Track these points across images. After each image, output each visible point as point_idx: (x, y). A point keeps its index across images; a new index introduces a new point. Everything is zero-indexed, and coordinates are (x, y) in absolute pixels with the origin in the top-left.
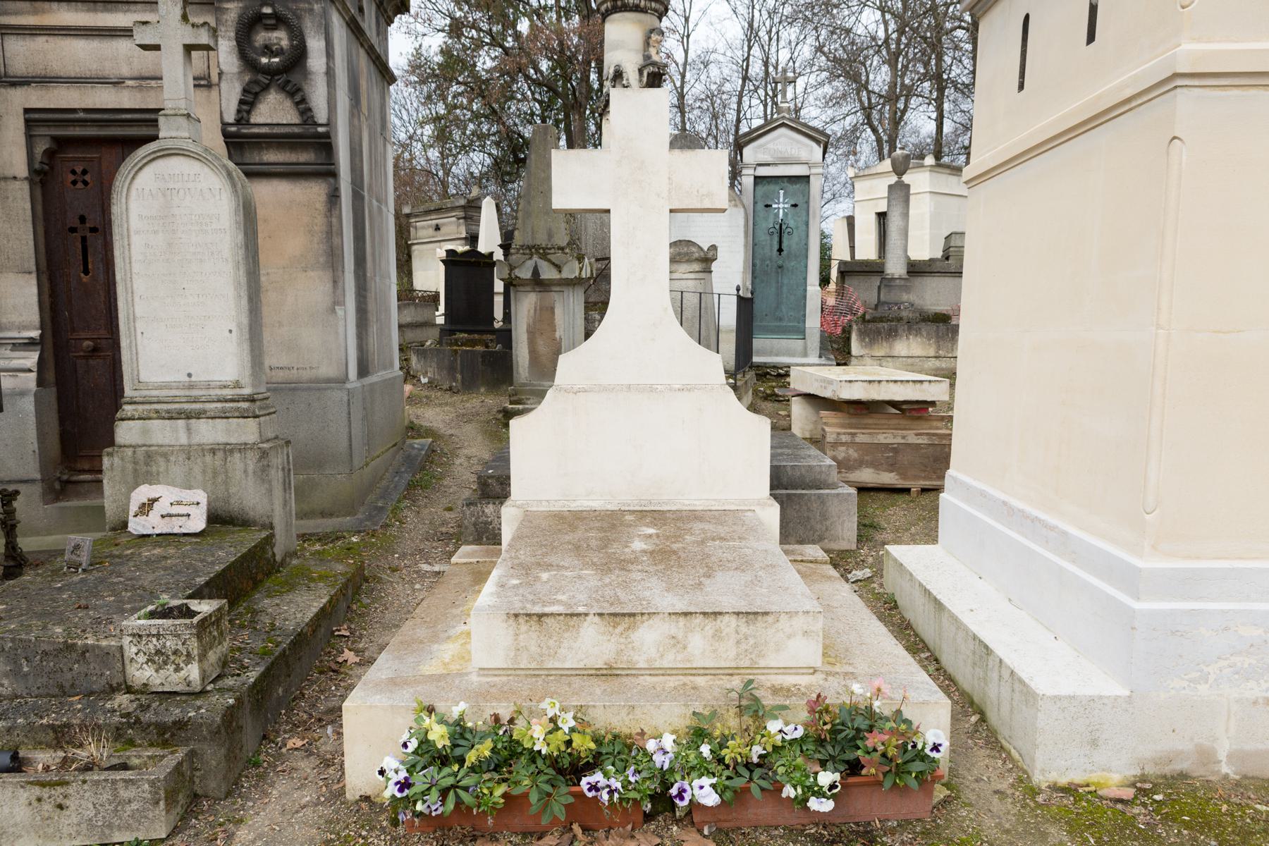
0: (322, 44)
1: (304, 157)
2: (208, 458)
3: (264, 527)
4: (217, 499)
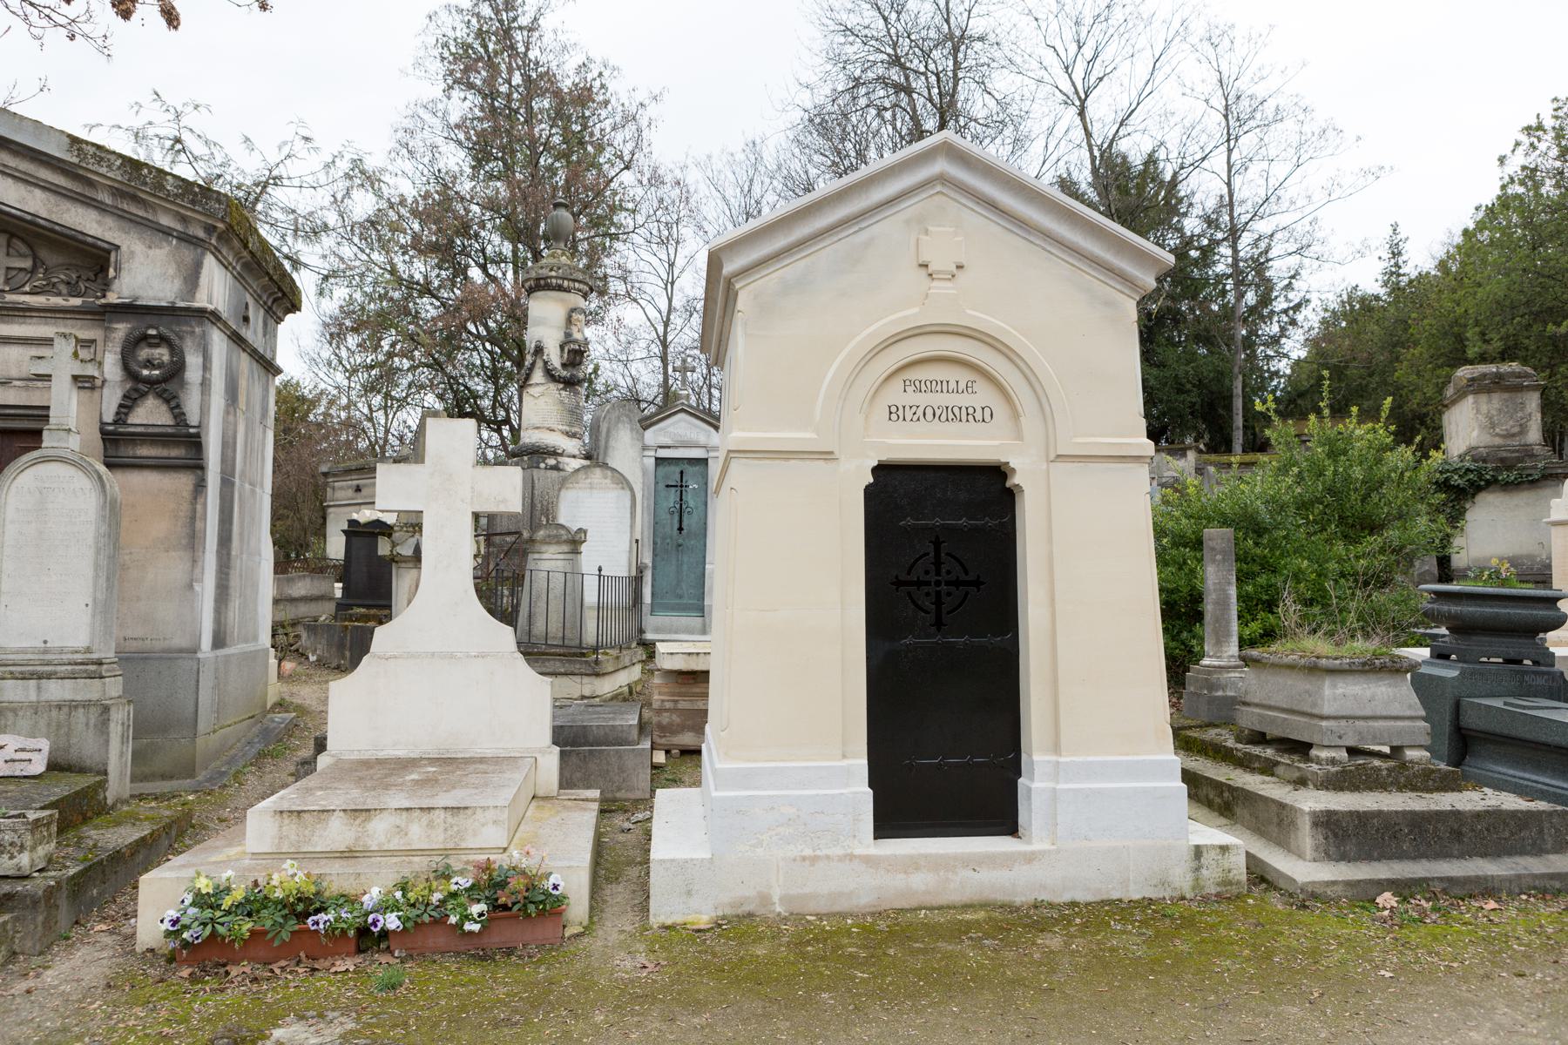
0: (200, 360)
1: (175, 452)
2: (54, 713)
3: (98, 773)
4: (58, 749)
